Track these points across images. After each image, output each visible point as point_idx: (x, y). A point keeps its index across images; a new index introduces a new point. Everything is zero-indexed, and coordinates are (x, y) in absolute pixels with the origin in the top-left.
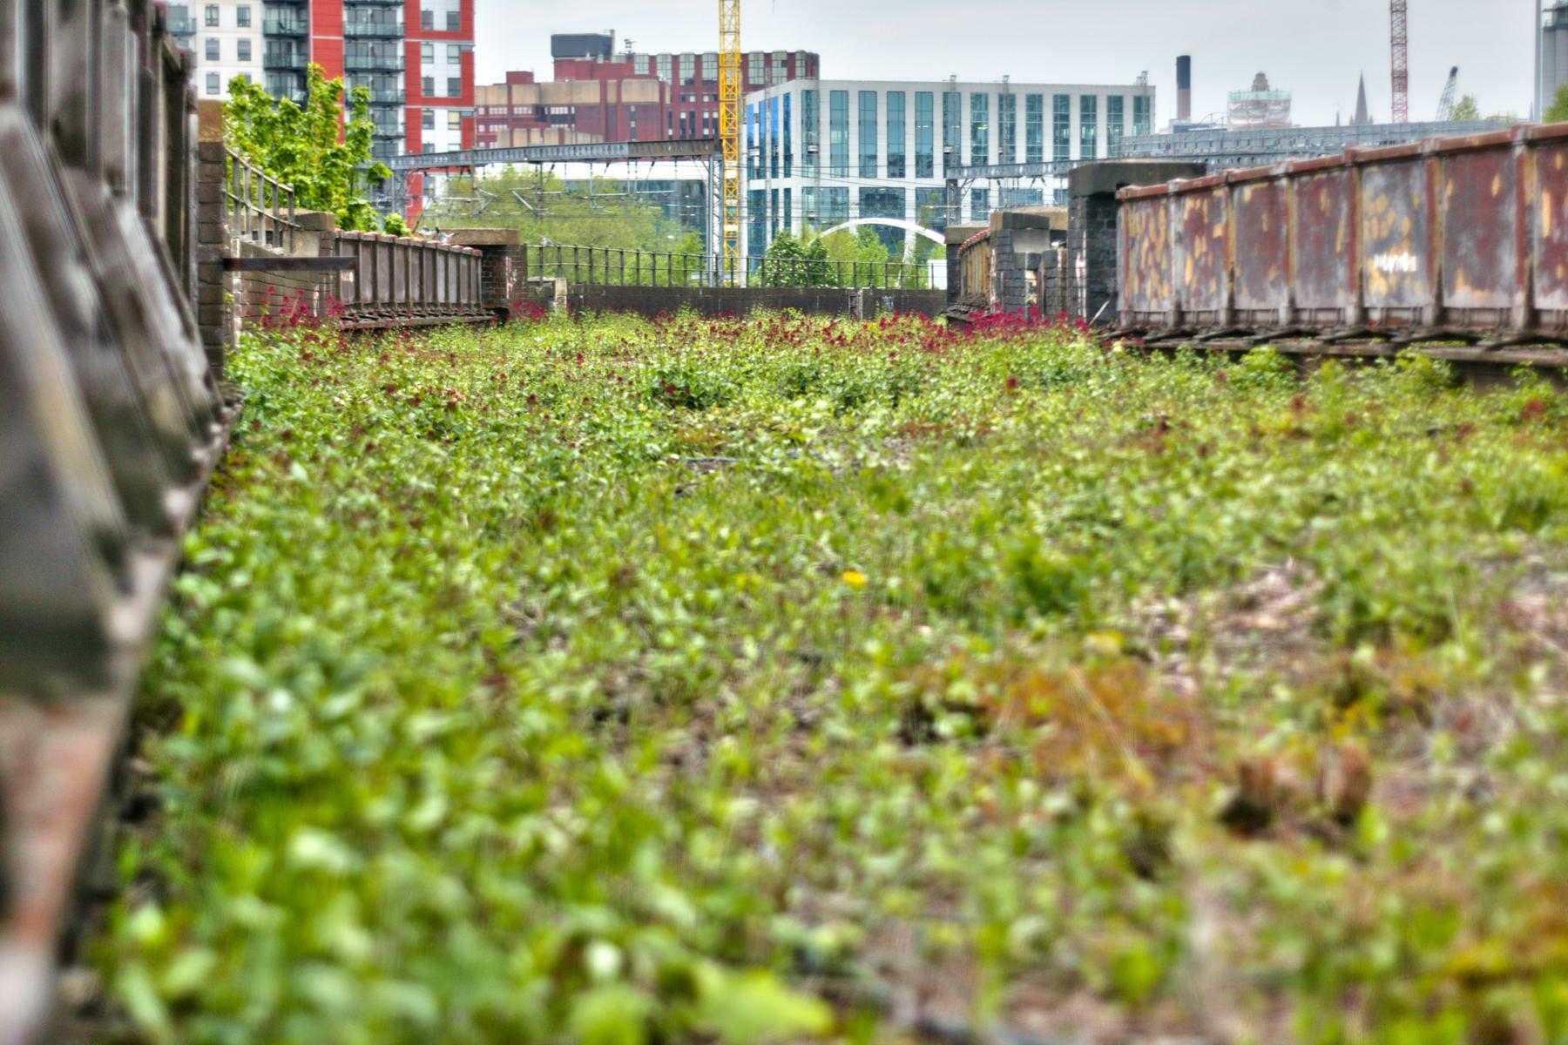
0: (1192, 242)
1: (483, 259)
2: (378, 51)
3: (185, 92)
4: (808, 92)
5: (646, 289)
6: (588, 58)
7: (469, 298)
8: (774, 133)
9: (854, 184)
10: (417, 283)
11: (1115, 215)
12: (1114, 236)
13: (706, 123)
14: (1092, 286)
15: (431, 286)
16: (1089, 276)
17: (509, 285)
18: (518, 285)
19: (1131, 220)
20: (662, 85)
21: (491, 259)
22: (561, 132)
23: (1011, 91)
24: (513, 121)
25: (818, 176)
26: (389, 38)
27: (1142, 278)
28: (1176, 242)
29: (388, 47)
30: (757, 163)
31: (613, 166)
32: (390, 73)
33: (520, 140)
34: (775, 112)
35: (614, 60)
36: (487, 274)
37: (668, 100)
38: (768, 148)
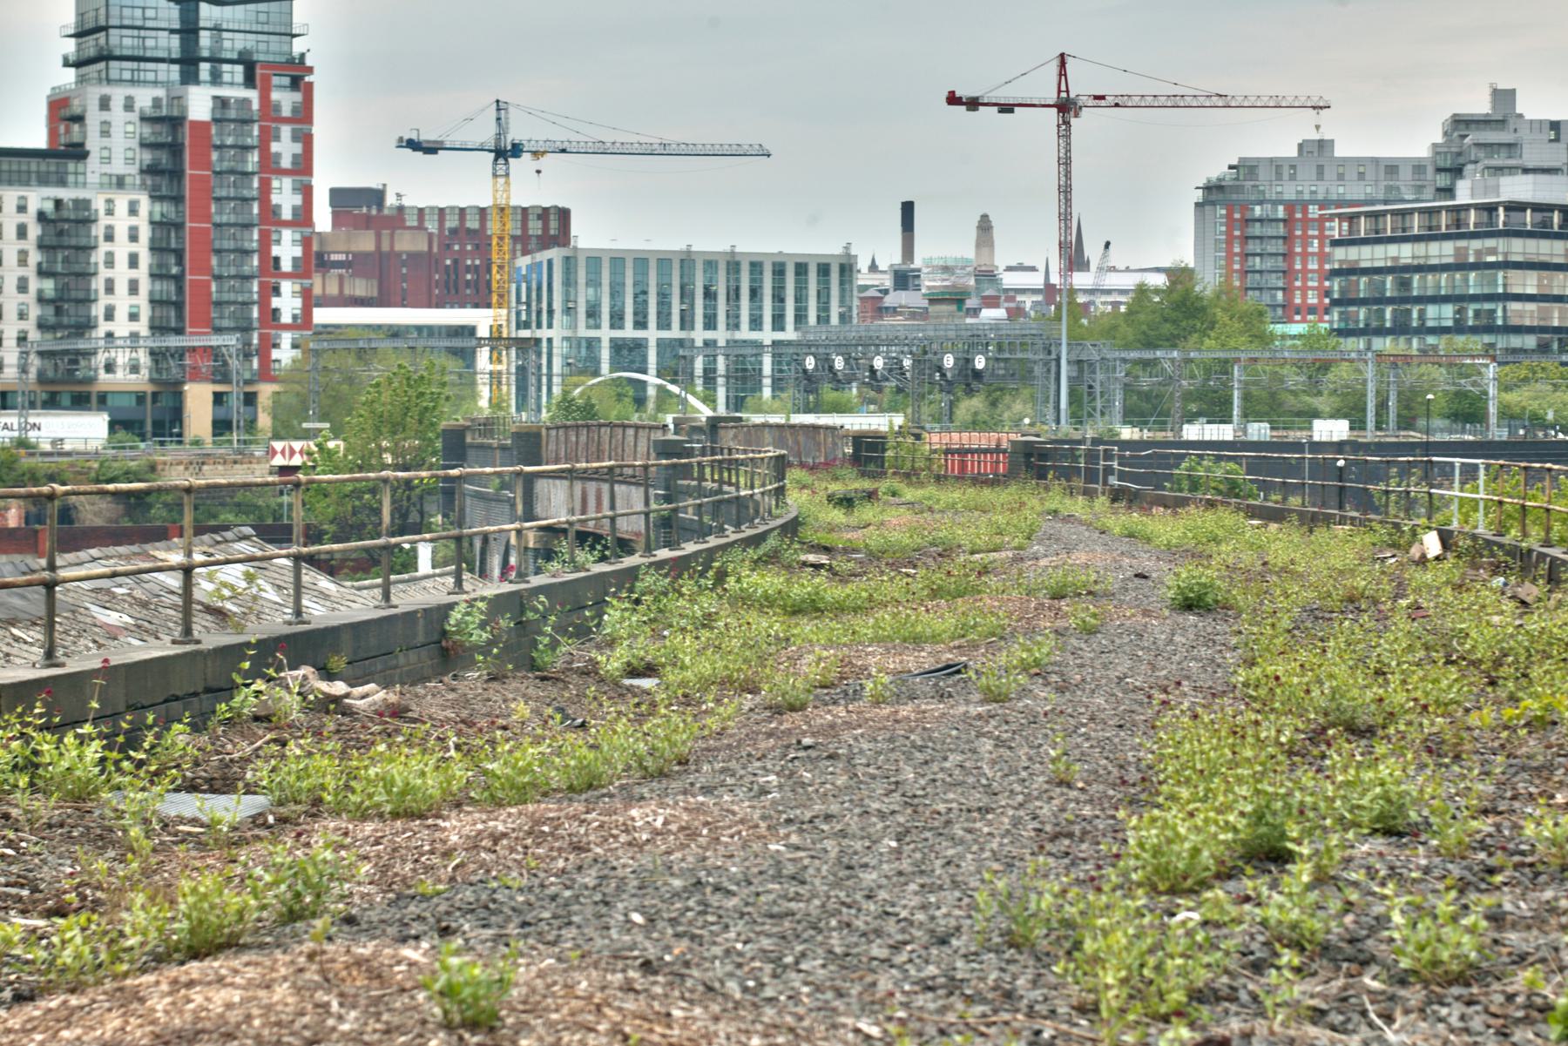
2: (238, 236)
4: (567, 258)
6: (365, 210)
19: (722, 432)
20: (431, 236)
22: (341, 277)
23: (737, 258)
26: (248, 226)
29: (246, 233)
30: (524, 317)
32: (247, 253)
34: (540, 273)
35: (386, 212)
37: (435, 249)
38: (534, 304)
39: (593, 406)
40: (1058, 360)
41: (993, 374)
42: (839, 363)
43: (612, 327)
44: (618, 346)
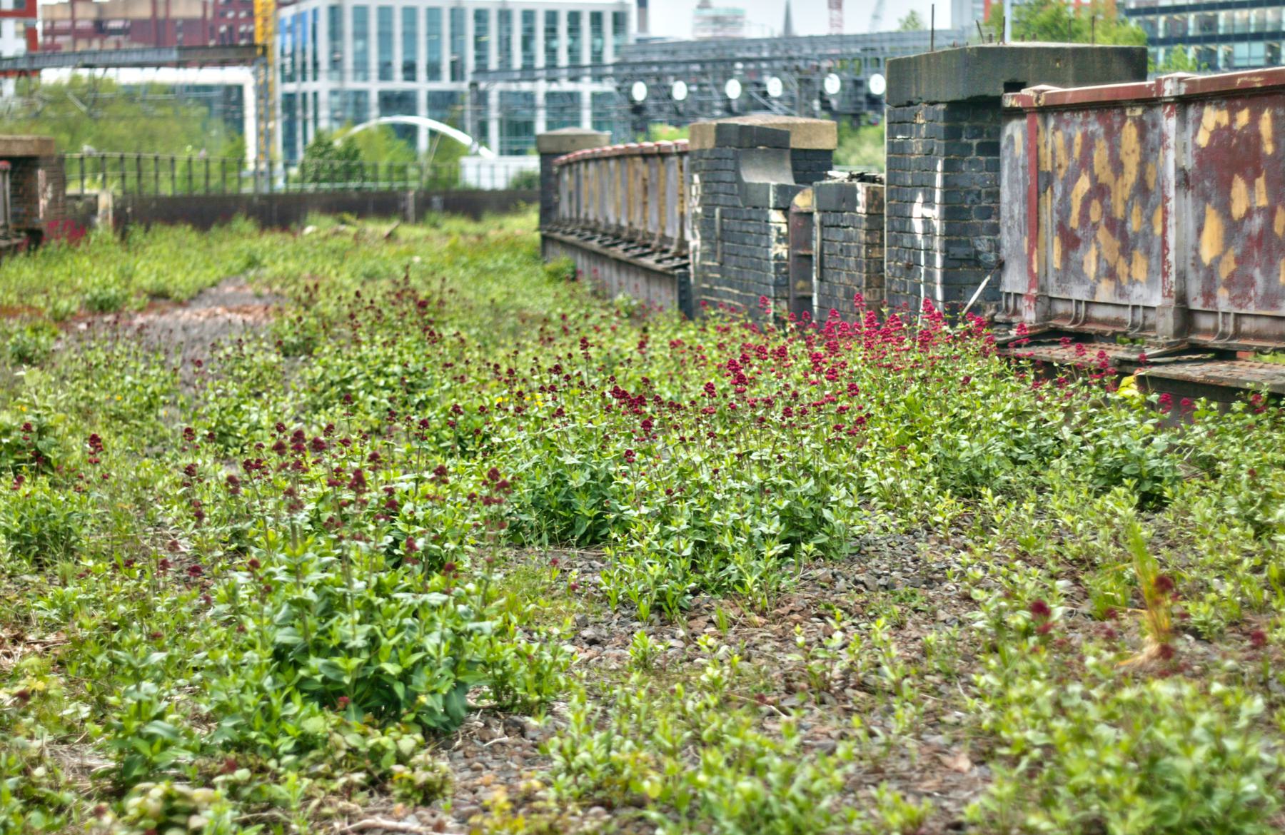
0: (1225, 187)
1: (12, 172)
5: (198, 199)
8: (304, 43)
9: (374, 87)
11: (998, 133)
12: (996, 167)
13: (242, 36)
14: (953, 250)
16: (948, 233)
17: (43, 203)
18: (54, 201)
21: (20, 172)
24: (76, 34)
25: (342, 79)
28: (1178, 186)
31: (163, 70)
33: (82, 46)
36: (17, 190)
42: (680, 91)
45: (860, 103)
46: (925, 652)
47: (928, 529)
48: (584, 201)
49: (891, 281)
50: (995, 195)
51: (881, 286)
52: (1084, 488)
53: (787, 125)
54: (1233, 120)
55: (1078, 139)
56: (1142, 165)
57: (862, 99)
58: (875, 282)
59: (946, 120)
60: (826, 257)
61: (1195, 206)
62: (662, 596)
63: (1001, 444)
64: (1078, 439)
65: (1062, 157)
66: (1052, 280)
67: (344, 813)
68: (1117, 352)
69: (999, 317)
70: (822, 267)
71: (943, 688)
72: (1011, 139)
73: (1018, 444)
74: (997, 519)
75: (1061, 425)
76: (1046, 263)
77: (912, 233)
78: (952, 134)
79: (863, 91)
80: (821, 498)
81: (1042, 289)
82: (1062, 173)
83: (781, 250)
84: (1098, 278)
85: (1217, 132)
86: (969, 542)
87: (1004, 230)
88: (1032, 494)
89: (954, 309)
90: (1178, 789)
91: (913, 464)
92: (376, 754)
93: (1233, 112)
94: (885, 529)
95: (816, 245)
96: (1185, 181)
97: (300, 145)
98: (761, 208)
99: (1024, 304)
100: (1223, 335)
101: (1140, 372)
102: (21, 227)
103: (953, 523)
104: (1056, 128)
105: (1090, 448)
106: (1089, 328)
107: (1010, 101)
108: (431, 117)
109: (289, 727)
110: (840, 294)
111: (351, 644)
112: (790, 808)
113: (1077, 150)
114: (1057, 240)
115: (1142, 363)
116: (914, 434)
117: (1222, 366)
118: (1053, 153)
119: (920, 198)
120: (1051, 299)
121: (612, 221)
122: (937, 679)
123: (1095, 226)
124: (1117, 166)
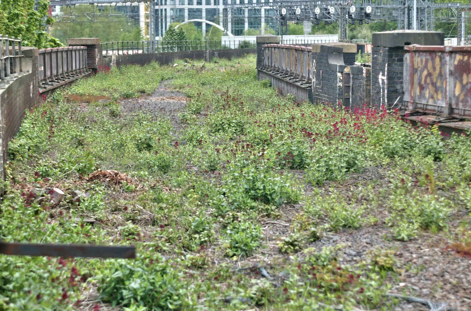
0: (461, 76)
1: (87, 50)
3: (59, 243)
7: (83, 66)
10: (66, 64)
11: (403, 56)
12: (402, 65)
14: (390, 88)
15: (71, 65)
16: (389, 84)
17: (97, 59)
21: (90, 50)
27: (422, 88)
28: (450, 75)
39: (183, 33)
40: (410, 9)
41: (375, 15)
43: (189, 4)
44: (208, 11)
45: (363, 16)
46: (379, 193)
47: (382, 166)
48: (274, 61)
49: (373, 96)
50: (402, 73)
51: (370, 97)
52: (421, 156)
53: (342, 45)
54: (463, 58)
55: (424, 60)
56: (441, 68)
57: (363, 14)
58: (368, 96)
59: (388, 52)
60: (354, 88)
61: (454, 80)
62: (318, 181)
63: (401, 144)
64: (420, 143)
65: (420, 65)
66: (417, 98)
67: (263, 220)
68: (432, 118)
69: (403, 108)
70: (353, 91)
71: (383, 200)
72: (406, 58)
73: (405, 144)
74: (398, 163)
75: (416, 139)
76: (415, 93)
77: (378, 83)
78: (390, 56)
79: (364, 11)
80: (355, 158)
81: (414, 100)
82: (420, 69)
83: (340, 84)
84: (429, 98)
85: (460, 61)
86: (391, 169)
87: (404, 84)
88: (408, 157)
89: (390, 105)
90: (427, 215)
91: (378, 149)
92: (267, 210)
93: (464, 56)
94: (370, 166)
95: (351, 84)
96: (451, 73)
97: (164, 32)
98: (334, 72)
99: (409, 104)
100: (461, 115)
101: (440, 124)
102: (90, 67)
103: (387, 164)
104: (418, 56)
105: (424, 145)
106: (426, 111)
107: (406, 48)
108: (206, 19)
109: (249, 204)
110: (358, 99)
111: (260, 188)
112: (352, 218)
113: (424, 63)
114: (418, 87)
115: (440, 122)
116: (379, 141)
117: (460, 123)
118: (417, 63)
119: (381, 73)
120: (417, 103)
121: (284, 68)
122: (382, 198)
123: (428, 84)
124: (434, 68)
